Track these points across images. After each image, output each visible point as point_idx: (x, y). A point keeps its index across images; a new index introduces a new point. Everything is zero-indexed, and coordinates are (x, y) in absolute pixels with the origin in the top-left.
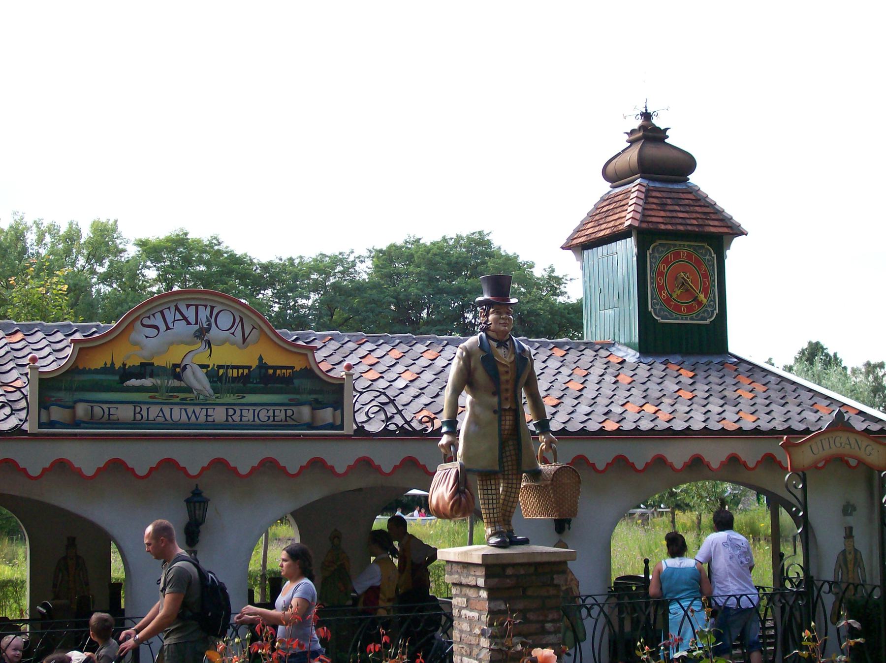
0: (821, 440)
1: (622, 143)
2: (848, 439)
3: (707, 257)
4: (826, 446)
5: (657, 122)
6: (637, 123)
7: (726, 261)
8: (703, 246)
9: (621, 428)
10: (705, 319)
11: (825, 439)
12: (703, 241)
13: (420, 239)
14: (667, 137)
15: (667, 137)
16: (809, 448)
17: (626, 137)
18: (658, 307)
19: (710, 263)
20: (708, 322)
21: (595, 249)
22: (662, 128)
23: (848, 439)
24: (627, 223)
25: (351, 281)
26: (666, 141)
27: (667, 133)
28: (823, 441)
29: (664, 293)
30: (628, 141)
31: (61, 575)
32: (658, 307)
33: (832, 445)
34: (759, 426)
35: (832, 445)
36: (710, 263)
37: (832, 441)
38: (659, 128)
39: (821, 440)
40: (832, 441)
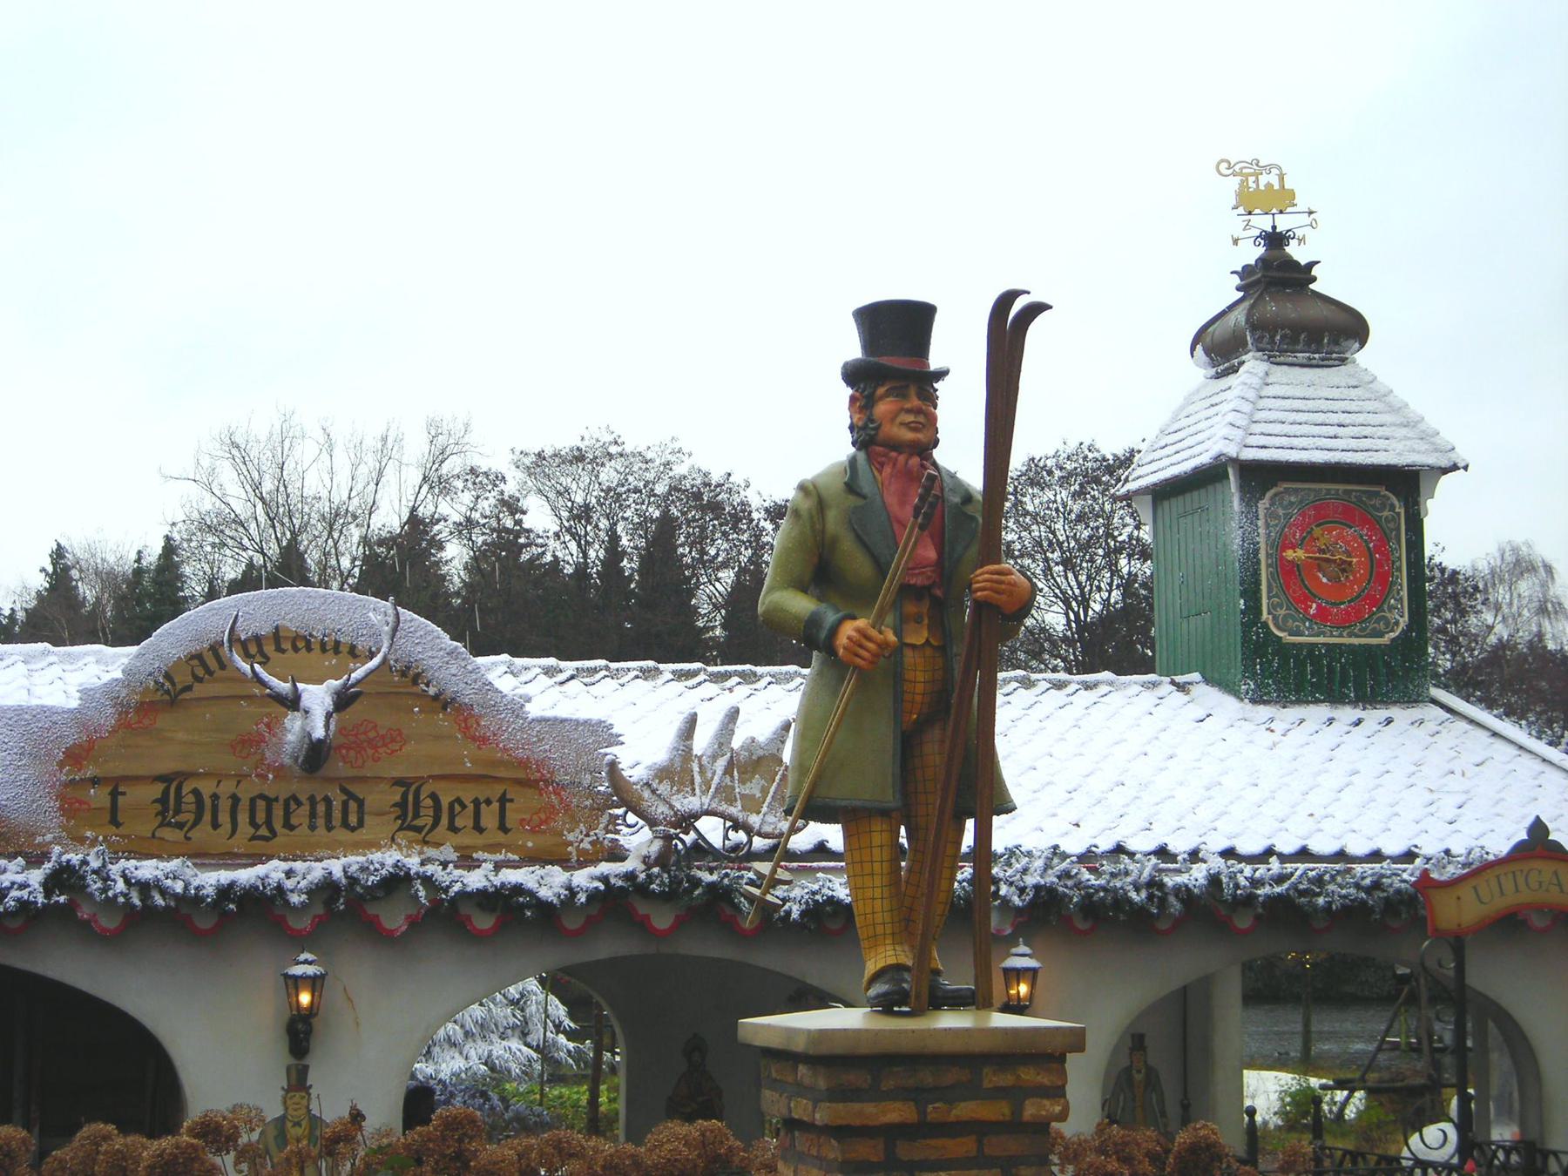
0: (1498, 877)
1: (1229, 292)
2: (1556, 873)
3: (1386, 513)
4: (1508, 885)
5: (1297, 252)
6: (1252, 253)
7: (1426, 520)
8: (1377, 494)
9: (1094, 849)
10: (1381, 635)
11: (1505, 874)
12: (1380, 484)
13: (620, 735)
14: (1314, 279)
15: (1314, 279)
16: (1473, 891)
17: (1236, 280)
18: (1282, 612)
19: (1391, 525)
20: (1386, 640)
21: (1188, 496)
22: (1303, 263)
23: (1556, 873)
24: (117, 1147)
25: (716, 607)
26: (1312, 286)
27: (1314, 272)
28: (1503, 879)
29: (1295, 584)
30: (1238, 289)
31: (1122, 1098)
32: (1282, 612)
33: (1522, 885)
34: (1416, 846)
35: (1522, 885)
36: (1391, 525)
37: (1521, 880)
38: (1297, 263)
39: (1498, 877)
40: (1521, 880)
